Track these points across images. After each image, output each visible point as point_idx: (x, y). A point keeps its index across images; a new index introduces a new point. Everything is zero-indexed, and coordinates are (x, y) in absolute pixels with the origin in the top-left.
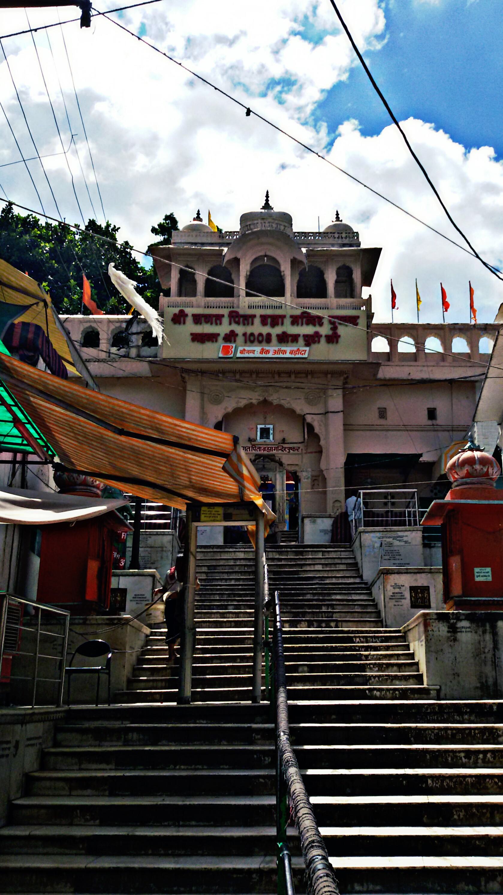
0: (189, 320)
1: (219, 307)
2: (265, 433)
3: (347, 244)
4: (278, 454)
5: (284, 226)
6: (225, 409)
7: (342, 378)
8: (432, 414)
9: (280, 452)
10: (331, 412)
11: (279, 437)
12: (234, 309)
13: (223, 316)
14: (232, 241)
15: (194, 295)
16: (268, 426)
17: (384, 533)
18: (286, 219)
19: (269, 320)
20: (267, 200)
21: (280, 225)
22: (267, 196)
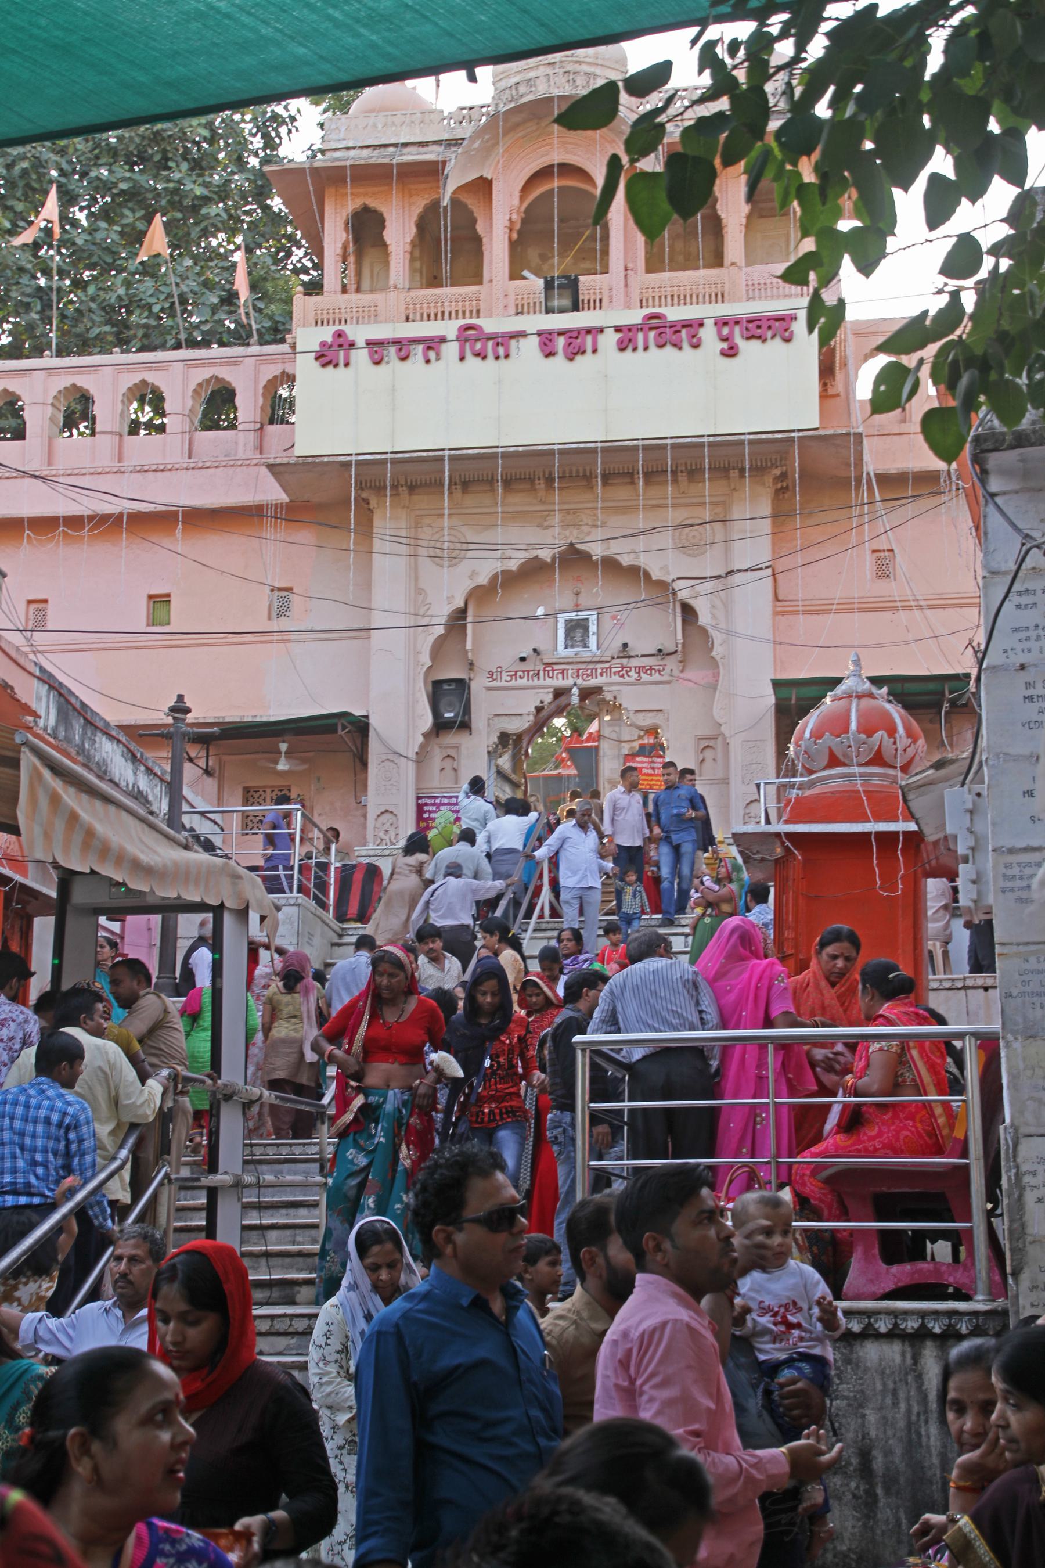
0: (361, 356)
2: (577, 630)
5: (587, 74)
6: (471, 577)
7: (769, 480)
8: (159, 602)
9: (616, 679)
10: (739, 571)
12: (474, 321)
13: (443, 340)
16: (583, 615)
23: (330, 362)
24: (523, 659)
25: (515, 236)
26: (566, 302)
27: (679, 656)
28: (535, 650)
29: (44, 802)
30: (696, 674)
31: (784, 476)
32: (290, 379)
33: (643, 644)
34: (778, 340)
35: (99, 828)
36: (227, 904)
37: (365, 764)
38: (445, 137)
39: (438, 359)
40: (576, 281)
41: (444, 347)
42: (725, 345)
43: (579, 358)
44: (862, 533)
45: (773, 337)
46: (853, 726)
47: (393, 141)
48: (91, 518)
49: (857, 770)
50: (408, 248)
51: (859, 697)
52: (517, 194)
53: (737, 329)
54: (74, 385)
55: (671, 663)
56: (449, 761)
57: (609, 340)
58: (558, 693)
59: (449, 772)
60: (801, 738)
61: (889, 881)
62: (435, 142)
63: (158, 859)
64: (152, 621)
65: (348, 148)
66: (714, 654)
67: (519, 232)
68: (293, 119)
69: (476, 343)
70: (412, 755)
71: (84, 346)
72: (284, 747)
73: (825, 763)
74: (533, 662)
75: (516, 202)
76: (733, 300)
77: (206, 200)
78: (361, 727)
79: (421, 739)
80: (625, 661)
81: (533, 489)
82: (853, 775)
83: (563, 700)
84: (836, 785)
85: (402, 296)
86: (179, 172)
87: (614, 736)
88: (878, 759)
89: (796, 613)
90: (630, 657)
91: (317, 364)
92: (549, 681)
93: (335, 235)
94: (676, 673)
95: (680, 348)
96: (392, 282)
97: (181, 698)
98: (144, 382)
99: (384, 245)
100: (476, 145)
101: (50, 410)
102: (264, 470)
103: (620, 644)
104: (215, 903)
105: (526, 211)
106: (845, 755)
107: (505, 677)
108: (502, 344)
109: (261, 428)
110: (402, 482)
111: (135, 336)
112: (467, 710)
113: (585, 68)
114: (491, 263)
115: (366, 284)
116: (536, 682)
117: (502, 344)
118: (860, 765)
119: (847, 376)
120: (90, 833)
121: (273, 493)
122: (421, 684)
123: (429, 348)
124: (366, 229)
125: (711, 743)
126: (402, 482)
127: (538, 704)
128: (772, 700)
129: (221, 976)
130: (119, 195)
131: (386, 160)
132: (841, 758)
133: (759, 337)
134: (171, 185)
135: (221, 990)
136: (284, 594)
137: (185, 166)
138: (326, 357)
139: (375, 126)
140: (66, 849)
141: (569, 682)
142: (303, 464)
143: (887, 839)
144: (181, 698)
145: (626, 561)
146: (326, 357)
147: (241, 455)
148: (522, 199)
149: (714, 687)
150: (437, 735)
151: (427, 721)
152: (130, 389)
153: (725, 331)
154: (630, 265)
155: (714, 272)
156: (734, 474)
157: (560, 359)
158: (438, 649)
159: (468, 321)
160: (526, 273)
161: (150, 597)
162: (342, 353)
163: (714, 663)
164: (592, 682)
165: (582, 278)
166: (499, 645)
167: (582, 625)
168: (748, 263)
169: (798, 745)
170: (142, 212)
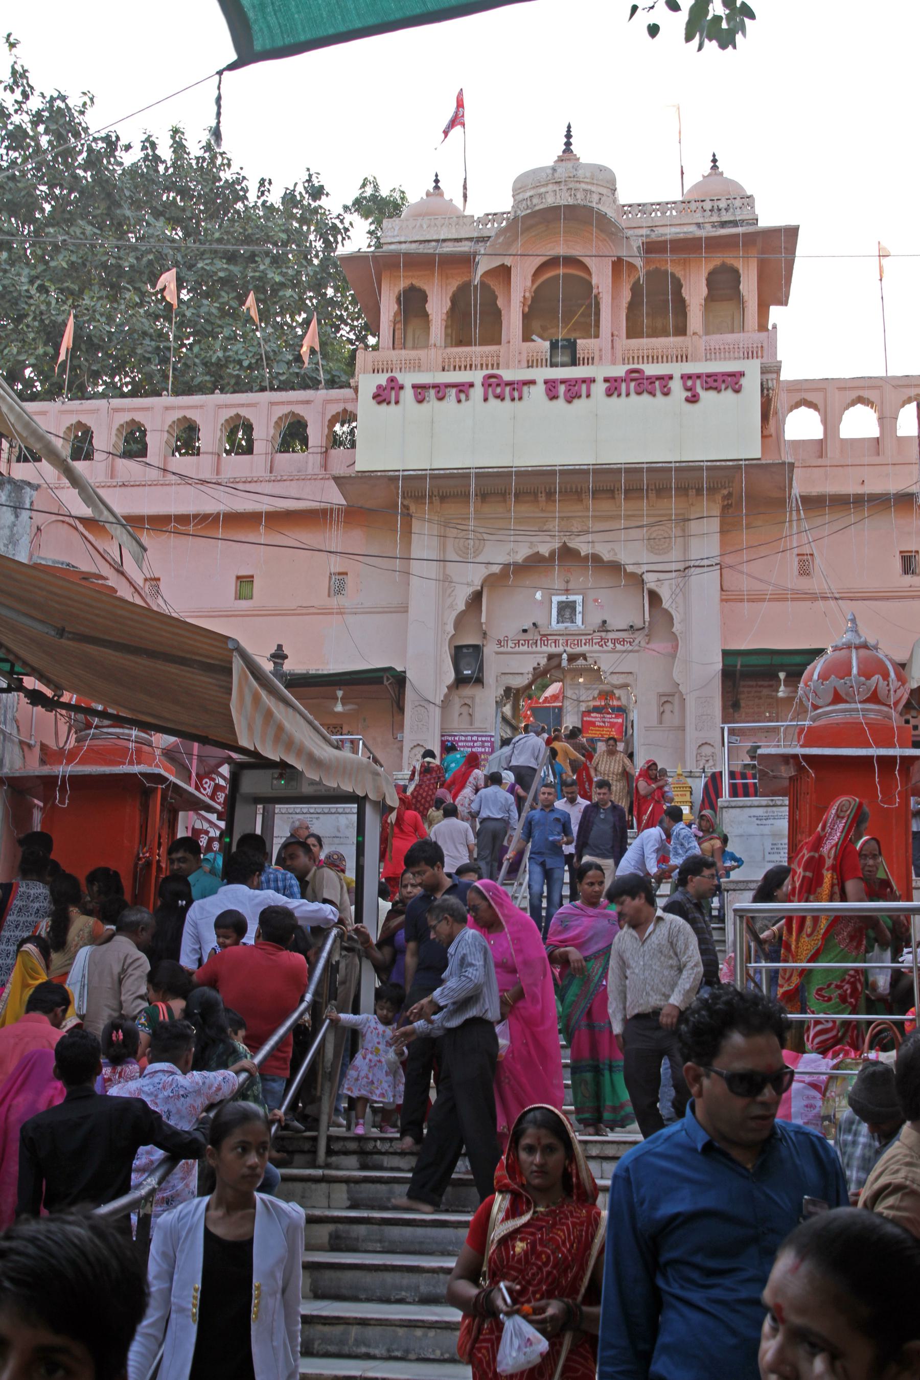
0: (408, 395)
1: (465, 367)
2: (567, 609)
3: (730, 222)
4: (592, 652)
7: (719, 498)
8: (245, 582)
9: (597, 647)
11: (595, 620)
12: (495, 372)
13: (471, 385)
14: (493, 234)
15: (743, 329)
16: (572, 598)
17: (770, 809)
18: (606, 180)
19: (562, 389)
20: (568, 144)
21: (591, 192)
22: (569, 136)
23: (384, 400)
24: (525, 631)
25: (527, 309)
26: (566, 359)
27: (646, 631)
28: (534, 624)
29: (248, 699)
30: (660, 645)
31: (730, 495)
32: (347, 417)
33: (618, 621)
34: (730, 391)
35: (287, 725)
36: (370, 796)
37: (401, 709)
38: (476, 235)
39: (467, 399)
40: (575, 343)
41: (472, 391)
42: (689, 394)
43: (576, 401)
44: (791, 541)
45: (726, 389)
46: (855, 671)
47: (435, 238)
48: (195, 516)
49: (859, 706)
50: (444, 317)
51: (857, 648)
52: (530, 278)
53: (698, 382)
54: (185, 417)
55: (639, 637)
56: (466, 708)
57: (599, 388)
58: (551, 657)
59: (465, 717)
60: (811, 679)
61: (888, 798)
62: (467, 239)
63: (326, 755)
64: (239, 596)
65: (400, 243)
66: (674, 630)
67: (530, 307)
68: (346, 230)
69: (496, 387)
70: (438, 702)
71: (188, 390)
72: (340, 694)
73: (830, 700)
74: (533, 633)
75: (529, 283)
76: (695, 360)
77: (282, 285)
78: (400, 680)
79: (446, 690)
80: (603, 634)
81: (536, 501)
82: (857, 710)
83: (554, 662)
84: (838, 718)
85: (440, 352)
86: (264, 265)
87: (574, 697)
88: (874, 698)
89: (742, 600)
90: (607, 631)
91: (374, 402)
92: (544, 648)
93: (388, 308)
94: (643, 644)
95: (654, 395)
96: (432, 341)
97: (280, 647)
98: (238, 415)
99: (426, 315)
100: (501, 240)
101: (166, 435)
102: (332, 483)
103: (600, 621)
104: (361, 794)
105: (536, 291)
106: (847, 694)
107: (510, 644)
108: (518, 388)
109: (326, 452)
110: (436, 493)
111: (228, 384)
112: (481, 669)
113: (584, 186)
114: (508, 328)
115: (409, 343)
116: (534, 649)
117: (518, 388)
118: (860, 702)
119: (778, 422)
120: (280, 728)
121: (335, 497)
122: (446, 648)
123: (461, 391)
124: (413, 304)
125: (670, 699)
126: (436, 493)
127: (535, 665)
128: (720, 666)
129: (363, 855)
130: (217, 281)
131: (431, 251)
132: (844, 696)
133: (716, 389)
134: (257, 274)
135: (363, 867)
136: (341, 577)
137: (267, 261)
138: (381, 397)
139: (421, 226)
140: (263, 741)
141: (560, 649)
142: (361, 477)
143: (887, 763)
144: (280, 647)
145: (606, 557)
146: (381, 397)
147: (310, 471)
148: (533, 282)
149: (673, 656)
150: (457, 688)
151: (451, 677)
152: (227, 421)
153: (689, 383)
154: (616, 333)
155: (680, 339)
156: (692, 493)
157: (561, 402)
158: (459, 623)
159: (490, 372)
160: (534, 337)
161: (238, 578)
162: (393, 393)
163: (674, 638)
164: (578, 650)
165: (578, 341)
166: (508, 617)
167: (571, 606)
168: (707, 332)
169: (806, 685)
170: (235, 294)
